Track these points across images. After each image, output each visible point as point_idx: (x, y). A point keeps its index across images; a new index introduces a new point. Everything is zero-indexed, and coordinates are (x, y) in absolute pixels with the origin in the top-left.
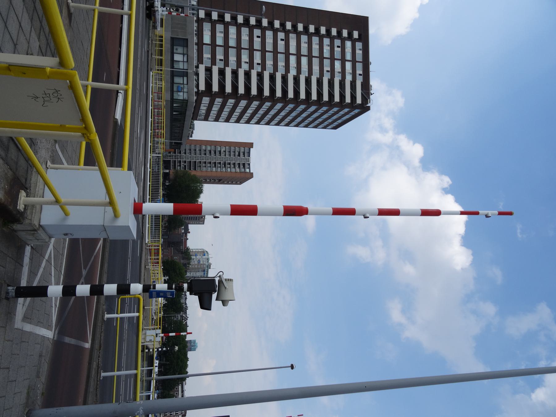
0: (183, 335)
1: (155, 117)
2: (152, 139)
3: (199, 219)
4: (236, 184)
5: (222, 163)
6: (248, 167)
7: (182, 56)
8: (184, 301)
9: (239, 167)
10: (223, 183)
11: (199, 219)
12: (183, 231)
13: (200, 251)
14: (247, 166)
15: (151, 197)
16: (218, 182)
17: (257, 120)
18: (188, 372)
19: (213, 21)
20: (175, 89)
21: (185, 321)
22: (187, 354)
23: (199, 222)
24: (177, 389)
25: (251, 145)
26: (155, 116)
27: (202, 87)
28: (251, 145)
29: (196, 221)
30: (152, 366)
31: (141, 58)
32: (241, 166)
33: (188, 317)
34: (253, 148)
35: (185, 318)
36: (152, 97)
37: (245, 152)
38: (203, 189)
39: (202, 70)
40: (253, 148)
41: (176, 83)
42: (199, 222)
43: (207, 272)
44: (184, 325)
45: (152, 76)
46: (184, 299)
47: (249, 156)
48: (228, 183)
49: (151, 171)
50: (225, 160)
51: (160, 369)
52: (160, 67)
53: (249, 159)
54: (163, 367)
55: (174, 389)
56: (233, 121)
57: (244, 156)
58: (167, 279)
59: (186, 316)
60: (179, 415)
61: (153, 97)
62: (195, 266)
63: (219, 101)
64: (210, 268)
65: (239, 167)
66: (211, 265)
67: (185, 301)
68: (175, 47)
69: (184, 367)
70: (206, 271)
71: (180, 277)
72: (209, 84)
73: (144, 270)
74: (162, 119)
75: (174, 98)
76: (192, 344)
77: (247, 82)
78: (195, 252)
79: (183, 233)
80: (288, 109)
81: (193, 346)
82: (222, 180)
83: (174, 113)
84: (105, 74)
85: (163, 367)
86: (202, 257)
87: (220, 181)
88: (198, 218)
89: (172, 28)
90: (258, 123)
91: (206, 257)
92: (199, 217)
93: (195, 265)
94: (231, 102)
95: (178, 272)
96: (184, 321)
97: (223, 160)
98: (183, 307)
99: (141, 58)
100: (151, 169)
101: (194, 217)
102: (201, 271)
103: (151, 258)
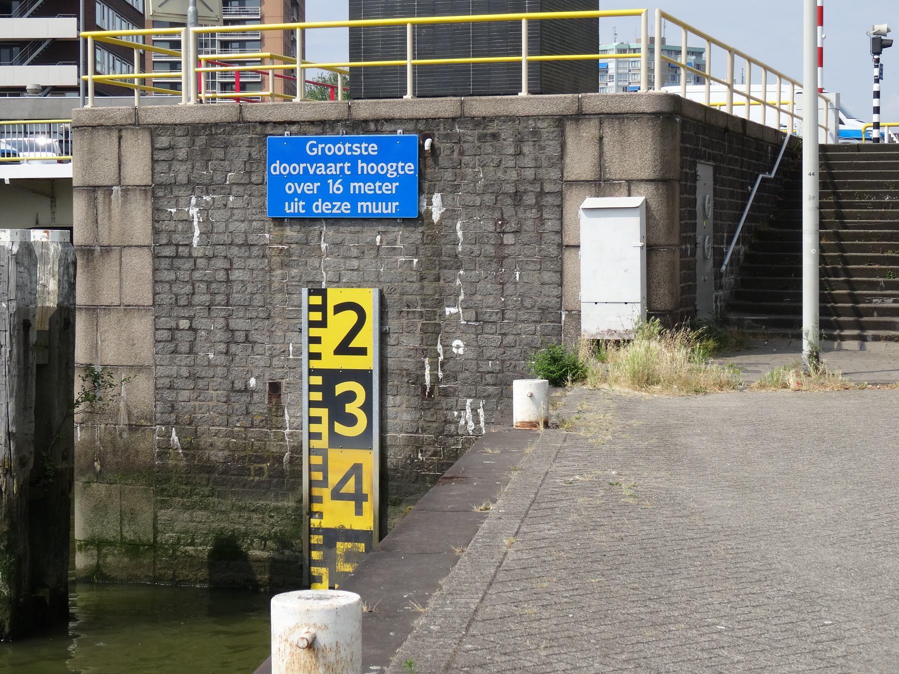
86: (611, 77)
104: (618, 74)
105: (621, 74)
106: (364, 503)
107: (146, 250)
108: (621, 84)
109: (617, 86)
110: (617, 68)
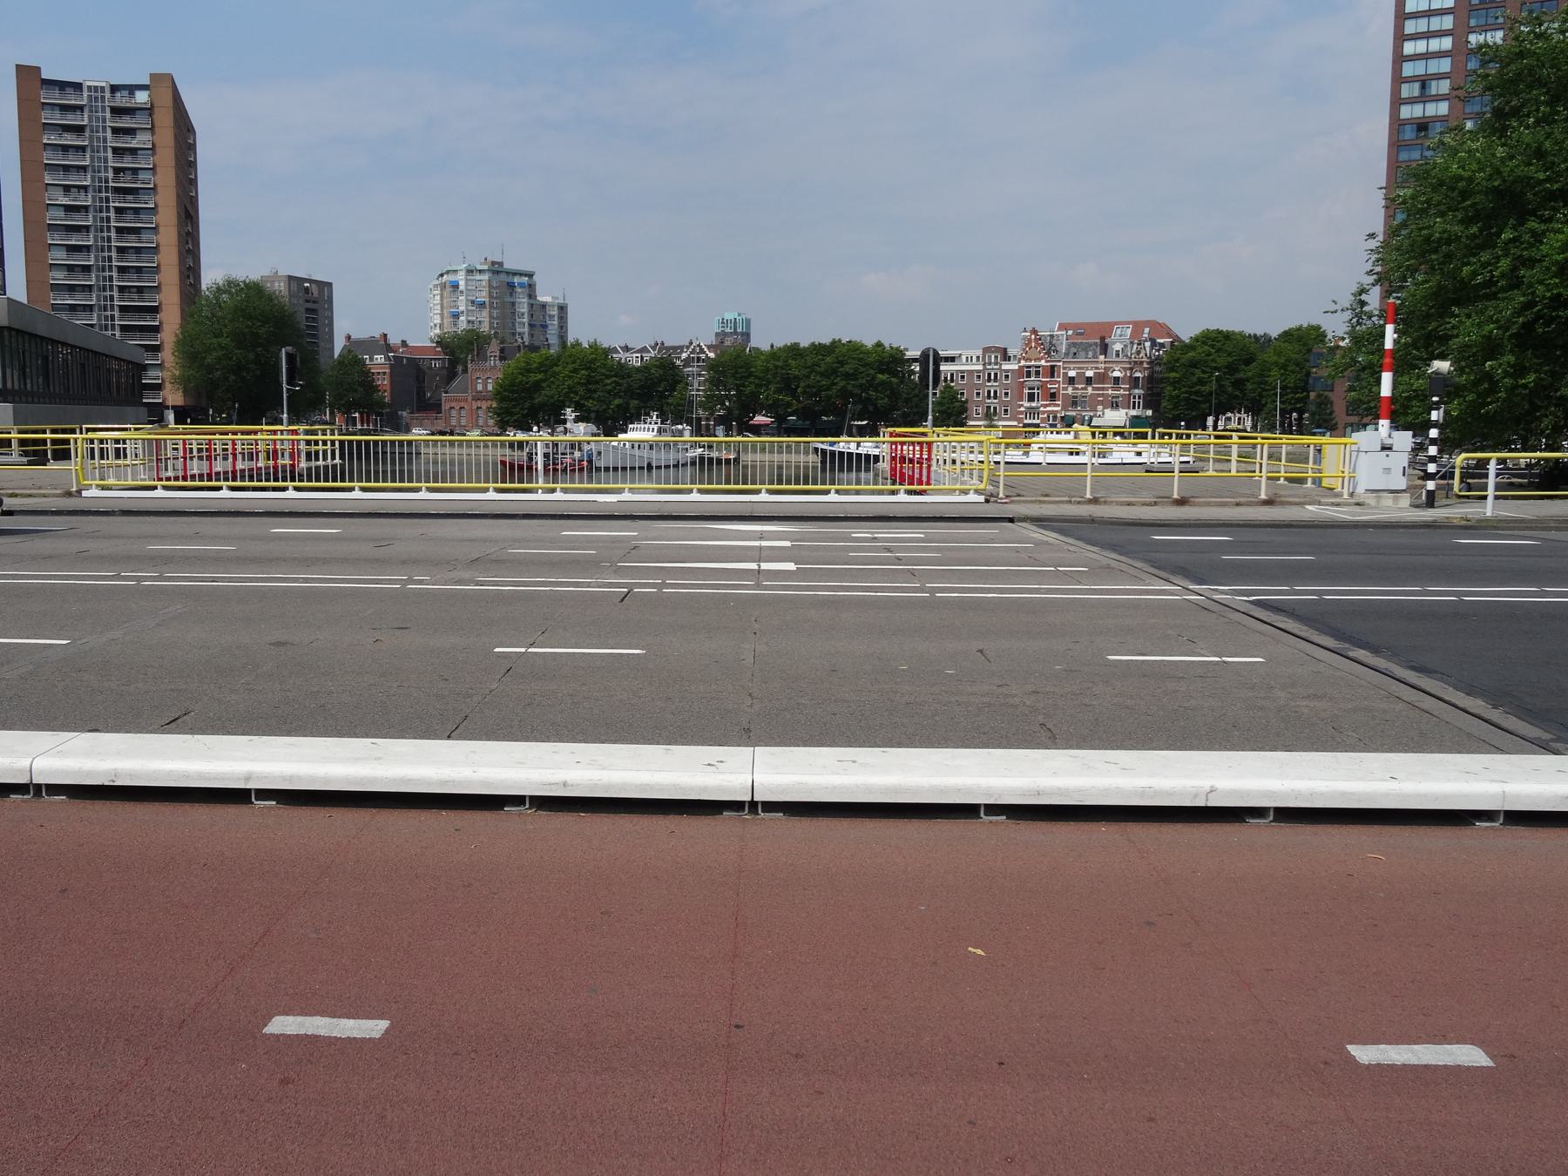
0: (1396, 342)
1: (218, 474)
2: (793, 487)
3: (314, 302)
8: (635, 355)
9: (131, 132)
12: (380, 358)
14: (121, 100)
15: (763, 483)
18: (876, 341)
21: (702, 351)
22: (820, 344)
25: (28, 76)
26: (234, 472)
28: (28, 76)
31: (219, 561)
32: (126, 122)
36: (165, 488)
38: (244, 282)
40: (38, 69)
43: (515, 274)
45: (104, 488)
46: (628, 355)
47: (78, 86)
49: (428, 485)
52: (1258, 460)
53: (89, 88)
60: (1000, 369)
61: (164, 483)
64: (501, 264)
65: (131, 132)
67: (635, 352)
69: (862, 356)
70: (510, 279)
71: (556, 369)
74: (235, 437)
76: (728, 330)
78: (442, 315)
79: (388, 358)
81: (735, 329)
86: (462, 292)
88: (309, 305)
91: (461, 278)
92: (307, 301)
93: (491, 317)
95: (540, 376)
96: (703, 356)
99: (219, 561)
100: (758, 487)
102: (511, 295)
104: (467, 290)
105: (470, 290)
106: (801, 346)
107: (29, 778)
108: (469, 298)
109: (467, 300)
110: (467, 285)
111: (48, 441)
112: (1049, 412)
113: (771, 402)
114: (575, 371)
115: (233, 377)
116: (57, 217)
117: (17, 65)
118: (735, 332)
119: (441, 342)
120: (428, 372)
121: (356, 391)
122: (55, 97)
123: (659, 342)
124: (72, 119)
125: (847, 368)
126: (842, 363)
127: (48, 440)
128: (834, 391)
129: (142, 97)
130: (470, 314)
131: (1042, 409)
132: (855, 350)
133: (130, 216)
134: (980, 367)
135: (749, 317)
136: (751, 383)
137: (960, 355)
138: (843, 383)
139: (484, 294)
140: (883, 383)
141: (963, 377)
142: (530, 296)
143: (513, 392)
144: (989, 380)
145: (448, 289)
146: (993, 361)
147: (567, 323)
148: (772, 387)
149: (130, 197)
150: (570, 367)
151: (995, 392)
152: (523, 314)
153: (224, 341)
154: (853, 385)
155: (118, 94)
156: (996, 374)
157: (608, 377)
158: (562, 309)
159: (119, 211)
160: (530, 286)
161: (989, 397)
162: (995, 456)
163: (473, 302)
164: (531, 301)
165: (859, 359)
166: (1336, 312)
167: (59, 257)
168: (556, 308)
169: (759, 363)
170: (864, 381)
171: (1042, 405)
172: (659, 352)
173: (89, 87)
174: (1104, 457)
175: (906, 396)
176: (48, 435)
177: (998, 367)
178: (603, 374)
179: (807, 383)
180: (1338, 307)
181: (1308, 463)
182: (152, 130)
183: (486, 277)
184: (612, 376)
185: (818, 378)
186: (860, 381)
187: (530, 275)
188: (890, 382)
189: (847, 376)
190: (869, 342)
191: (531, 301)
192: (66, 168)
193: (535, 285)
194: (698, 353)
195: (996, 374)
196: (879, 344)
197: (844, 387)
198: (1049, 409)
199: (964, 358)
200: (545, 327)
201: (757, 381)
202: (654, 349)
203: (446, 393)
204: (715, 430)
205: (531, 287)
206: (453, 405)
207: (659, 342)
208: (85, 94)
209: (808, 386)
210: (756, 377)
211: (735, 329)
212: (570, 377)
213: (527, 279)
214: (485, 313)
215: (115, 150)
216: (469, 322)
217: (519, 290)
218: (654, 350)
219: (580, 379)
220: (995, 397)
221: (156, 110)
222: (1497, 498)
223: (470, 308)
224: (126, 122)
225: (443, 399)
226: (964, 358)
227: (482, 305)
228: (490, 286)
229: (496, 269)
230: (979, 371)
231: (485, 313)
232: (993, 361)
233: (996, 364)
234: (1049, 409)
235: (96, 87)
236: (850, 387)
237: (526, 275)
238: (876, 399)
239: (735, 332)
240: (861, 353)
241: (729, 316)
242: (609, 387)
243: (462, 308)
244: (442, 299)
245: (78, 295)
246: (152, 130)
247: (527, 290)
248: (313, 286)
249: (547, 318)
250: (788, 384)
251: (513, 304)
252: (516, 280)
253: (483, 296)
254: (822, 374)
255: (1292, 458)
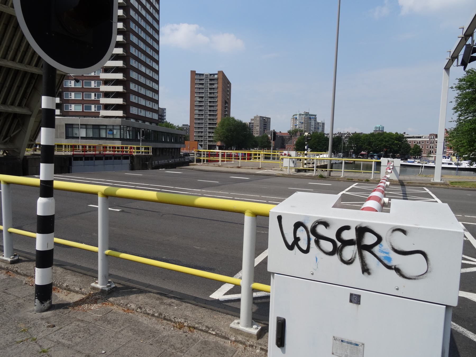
3: (266, 122)
4: (230, 87)
5: (209, 100)
6: (213, 76)
7: (92, 129)
9: (213, 84)
10: (229, 99)
11: (266, 122)
13: (292, 121)
14: (212, 77)
16: (228, 104)
17: (153, 63)
19: (61, 102)
20: (111, 137)
23: (268, 122)
24: (410, 142)
25: (193, 73)
27: (120, 113)
28: (193, 73)
29: (267, 125)
30: (93, 151)
32: (212, 82)
33: (348, 132)
34: (195, 71)
35: (348, 135)
37: (199, 79)
39: (103, 113)
40: (195, 71)
41: (99, 135)
42: (268, 122)
43: (311, 115)
44: (353, 135)
47: (203, 75)
48: (230, 95)
50: (207, 98)
51: (390, 156)
54: (388, 154)
55: (409, 145)
56: (157, 86)
57: (203, 79)
58: (310, 149)
59: (347, 133)
62: (305, 126)
63: (133, 99)
64: (308, 113)
65: (213, 84)
66: (306, 112)
68: (75, 136)
69: (391, 136)
70: (310, 116)
72: (117, 107)
73: (222, 168)
75: (119, 138)
76: (377, 130)
77: (111, 71)
78: (293, 125)
80: (136, 29)
81: (379, 129)
82: (225, 101)
83: (173, 141)
84: (152, 195)
85: (388, 154)
86: (298, 120)
87: (227, 103)
89: (58, 138)
90: (157, 62)
91: (298, 117)
92: (264, 122)
93: (304, 126)
94: (133, 86)
97: (207, 99)
98: (338, 136)
101: (264, 126)
103: (222, 161)
109: (299, 122)
110: (299, 118)
111: (258, 154)
112: (449, 153)
113: (365, 148)
114: (315, 139)
115: (225, 139)
116: (197, 103)
117: (191, 71)
118: (379, 130)
119: (289, 132)
120: (285, 139)
121: (265, 143)
122: (198, 77)
123: (339, 132)
124: (201, 82)
125: (387, 139)
126: (385, 138)
127: (246, 154)
128: (382, 145)
129: (216, 76)
130: (299, 125)
131: (447, 152)
132: (389, 135)
133: (212, 103)
134: (428, 140)
135: (383, 126)
136: (360, 143)
137: (423, 136)
138: (384, 143)
139: (303, 120)
140: (396, 144)
141: (423, 142)
142: (315, 121)
143: (300, 144)
144: (431, 143)
145: (295, 119)
146: (432, 138)
147: (324, 127)
148: (366, 144)
149: (212, 99)
150: (314, 138)
151: (433, 147)
152: (313, 125)
153: (224, 130)
154: (387, 144)
155: (211, 76)
156: (433, 142)
157: (323, 141)
158: (323, 124)
159: (210, 102)
160: (315, 118)
161: (431, 148)
162: (425, 164)
163: (300, 122)
164: (315, 122)
165: (390, 137)
166: (452, 121)
167: (197, 112)
168: (321, 124)
169: (363, 138)
170: (390, 143)
171: (447, 151)
172: (339, 135)
173: (205, 75)
174: (460, 166)
175: (403, 147)
176: (271, 153)
177: (434, 140)
178: (322, 140)
179: (375, 143)
180: (452, 120)
181: (225, 157)
182: (218, 83)
183: (304, 116)
184: (325, 141)
185: (378, 142)
186: (389, 143)
187: (315, 116)
188: (399, 143)
189: (386, 141)
190: (394, 132)
191: (315, 122)
192: (200, 93)
193: (316, 118)
194: (349, 135)
195: (433, 142)
196: (397, 133)
197: (385, 144)
198: (449, 152)
199: (424, 137)
200: (318, 128)
201: (361, 142)
202: (338, 134)
203: (287, 144)
204: (352, 155)
205: (315, 118)
206: (288, 147)
207: (339, 132)
208: (204, 76)
209: (375, 144)
210: (361, 141)
211: (379, 129)
212: (314, 141)
213: (314, 116)
214: (303, 125)
215: (210, 88)
216: (299, 127)
217: (312, 119)
218: (338, 134)
219: (316, 141)
220: (433, 148)
221: (219, 79)
222: (344, 171)
223: (300, 124)
224: (212, 82)
225: (286, 146)
226: (424, 137)
227: (303, 123)
228: (305, 118)
229: (307, 114)
230: (428, 141)
231: (303, 125)
232: (432, 138)
233: (433, 139)
234: (449, 152)
235: (207, 75)
236: (386, 145)
237: (314, 116)
238: (394, 148)
239: (379, 130)
240: (391, 135)
241: (378, 126)
242: (323, 143)
243: (298, 124)
244: (293, 121)
245: (200, 120)
246: (218, 83)
247: (314, 119)
248: (266, 119)
249: (319, 126)
250: (370, 144)
251: (310, 123)
252: (312, 117)
253: (303, 121)
254: (379, 141)
255: (139, 152)
